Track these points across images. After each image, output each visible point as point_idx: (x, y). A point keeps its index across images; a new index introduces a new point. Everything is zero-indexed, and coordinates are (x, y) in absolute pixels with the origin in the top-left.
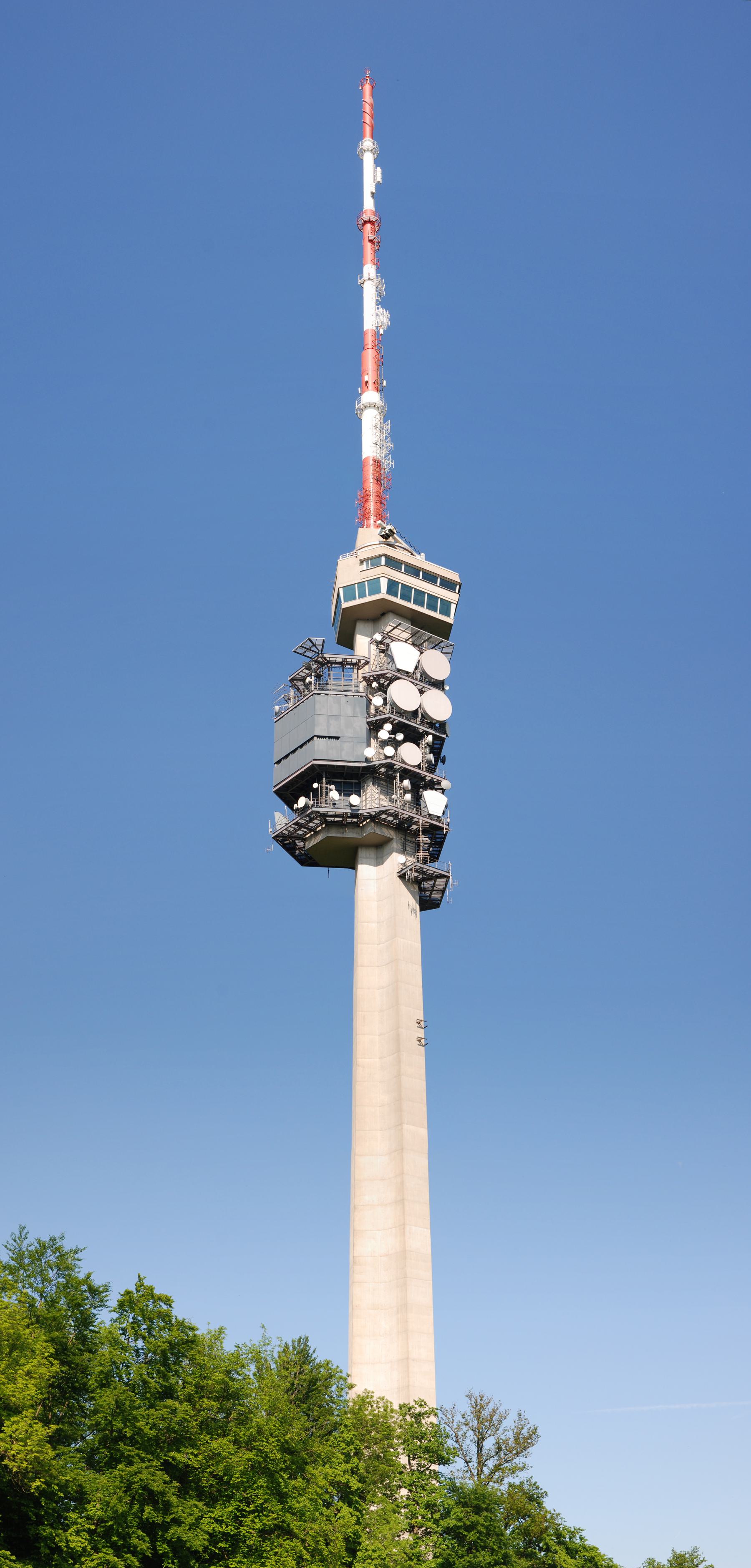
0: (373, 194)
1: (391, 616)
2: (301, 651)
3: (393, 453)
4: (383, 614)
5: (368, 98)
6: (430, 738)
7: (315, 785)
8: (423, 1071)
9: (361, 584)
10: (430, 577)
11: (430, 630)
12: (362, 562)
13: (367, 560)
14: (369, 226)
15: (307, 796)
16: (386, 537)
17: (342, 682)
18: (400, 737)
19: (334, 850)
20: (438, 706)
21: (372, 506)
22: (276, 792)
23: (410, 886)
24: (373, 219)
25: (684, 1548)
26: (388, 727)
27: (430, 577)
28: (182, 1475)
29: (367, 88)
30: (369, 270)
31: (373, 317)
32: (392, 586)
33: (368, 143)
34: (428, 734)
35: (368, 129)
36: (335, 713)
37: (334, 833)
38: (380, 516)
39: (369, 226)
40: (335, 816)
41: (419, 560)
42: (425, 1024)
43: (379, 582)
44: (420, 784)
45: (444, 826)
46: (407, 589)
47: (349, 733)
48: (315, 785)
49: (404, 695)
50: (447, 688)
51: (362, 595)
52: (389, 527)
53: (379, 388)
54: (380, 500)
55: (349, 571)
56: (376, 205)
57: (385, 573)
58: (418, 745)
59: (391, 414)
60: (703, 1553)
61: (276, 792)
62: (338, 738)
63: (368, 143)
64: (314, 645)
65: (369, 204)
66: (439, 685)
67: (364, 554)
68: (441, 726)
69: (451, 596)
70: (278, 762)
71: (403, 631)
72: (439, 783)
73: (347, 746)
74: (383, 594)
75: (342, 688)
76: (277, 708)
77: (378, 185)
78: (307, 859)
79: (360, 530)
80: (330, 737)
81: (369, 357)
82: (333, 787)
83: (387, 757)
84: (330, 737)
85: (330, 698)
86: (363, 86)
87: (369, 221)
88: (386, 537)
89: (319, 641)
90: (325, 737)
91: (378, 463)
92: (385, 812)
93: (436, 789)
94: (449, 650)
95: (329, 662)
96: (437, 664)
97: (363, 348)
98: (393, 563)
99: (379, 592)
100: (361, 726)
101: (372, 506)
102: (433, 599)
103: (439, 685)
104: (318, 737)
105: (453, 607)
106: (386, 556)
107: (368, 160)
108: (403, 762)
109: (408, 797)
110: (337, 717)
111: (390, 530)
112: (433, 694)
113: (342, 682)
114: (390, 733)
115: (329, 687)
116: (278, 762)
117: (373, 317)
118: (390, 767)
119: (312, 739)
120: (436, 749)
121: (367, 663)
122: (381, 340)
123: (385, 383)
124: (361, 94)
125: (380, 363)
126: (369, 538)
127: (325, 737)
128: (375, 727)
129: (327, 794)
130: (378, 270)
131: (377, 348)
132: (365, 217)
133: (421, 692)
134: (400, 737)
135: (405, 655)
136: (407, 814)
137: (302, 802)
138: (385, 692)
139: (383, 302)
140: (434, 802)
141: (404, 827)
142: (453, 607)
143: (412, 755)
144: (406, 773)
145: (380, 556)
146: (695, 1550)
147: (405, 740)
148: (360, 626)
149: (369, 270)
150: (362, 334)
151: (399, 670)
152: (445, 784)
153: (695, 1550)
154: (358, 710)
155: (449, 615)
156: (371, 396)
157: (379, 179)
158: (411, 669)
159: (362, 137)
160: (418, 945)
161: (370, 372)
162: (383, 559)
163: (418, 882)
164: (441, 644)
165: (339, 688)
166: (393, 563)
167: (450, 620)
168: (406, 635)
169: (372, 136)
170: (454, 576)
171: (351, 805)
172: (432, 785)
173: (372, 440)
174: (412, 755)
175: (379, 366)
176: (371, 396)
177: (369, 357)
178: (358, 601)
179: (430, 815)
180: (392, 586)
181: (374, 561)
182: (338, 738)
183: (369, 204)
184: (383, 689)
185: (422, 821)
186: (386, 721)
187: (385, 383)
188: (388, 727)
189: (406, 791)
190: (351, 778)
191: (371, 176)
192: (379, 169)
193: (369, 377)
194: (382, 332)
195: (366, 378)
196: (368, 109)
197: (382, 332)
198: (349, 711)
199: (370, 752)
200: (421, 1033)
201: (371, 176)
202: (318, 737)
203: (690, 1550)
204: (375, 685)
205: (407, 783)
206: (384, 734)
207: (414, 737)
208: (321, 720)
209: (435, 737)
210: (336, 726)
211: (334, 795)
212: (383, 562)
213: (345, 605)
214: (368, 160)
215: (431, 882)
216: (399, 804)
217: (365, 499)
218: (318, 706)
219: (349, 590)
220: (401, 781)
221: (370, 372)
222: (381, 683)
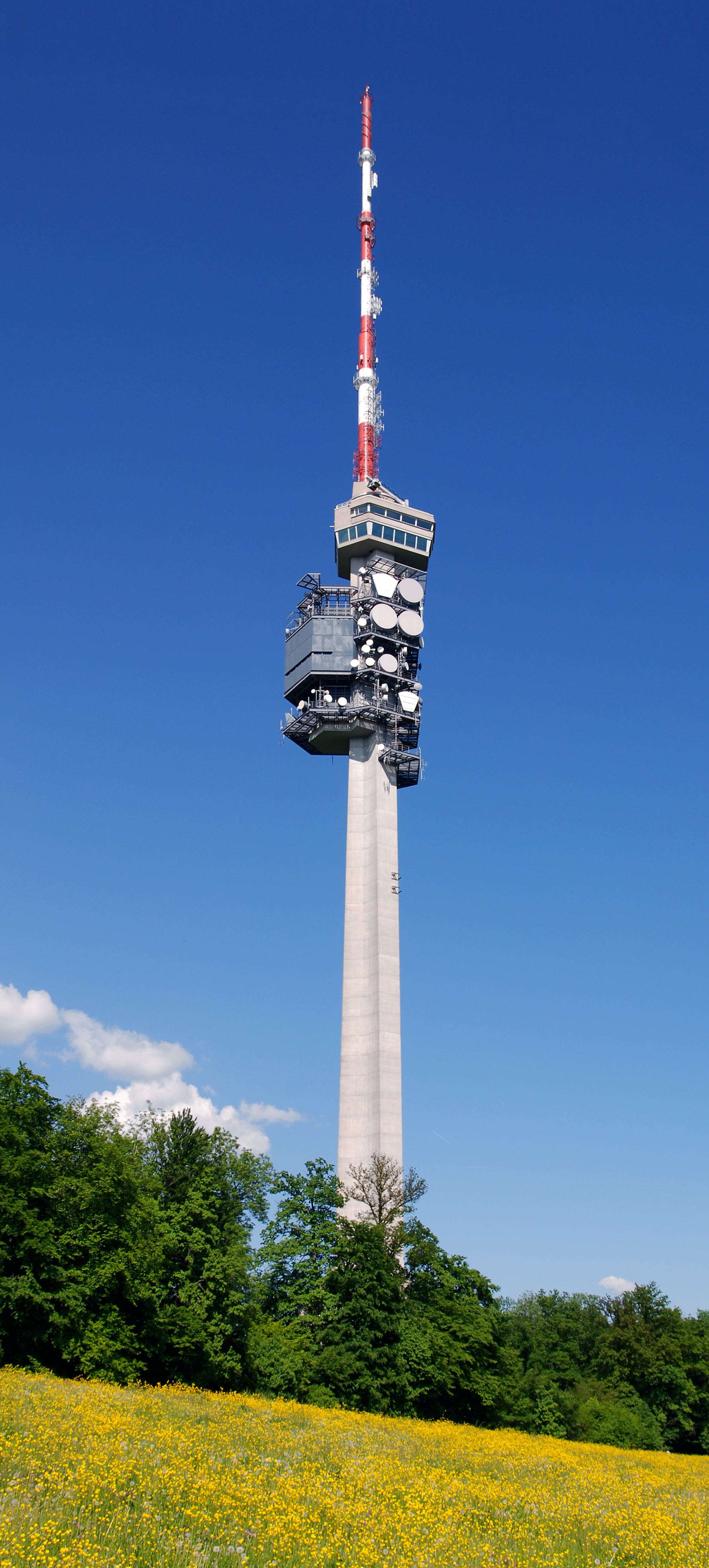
0: (369, 198)
1: (377, 551)
2: (304, 584)
3: (384, 419)
4: (371, 552)
5: (367, 112)
6: (405, 650)
7: (313, 691)
8: (397, 913)
9: (352, 529)
10: (409, 520)
11: (408, 562)
12: (352, 510)
13: (356, 508)
14: (366, 226)
15: (306, 700)
16: (373, 488)
17: (337, 608)
18: (381, 650)
19: (331, 742)
20: (413, 624)
21: (366, 464)
22: (287, 697)
23: (388, 767)
24: (369, 219)
25: (644, 1282)
26: (370, 642)
27: (409, 520)
28: (43, 1207)
29: (367, 101)
30: (366, 264)
31: (369, 304)
32: (377, 528)
33: (366, 152)
34: (403, 646)
35: (367, 140)
36: (329, 633)
37: (327, 728)
38: (372, 474)
39: (366, 226)
40: (328, 715)
41: (404, 507)
42: (402, 876)
43: (366, 526)
44: (395, 686)
45: (416, 720)
46: (389, 530)
47: (339, 649)
48: (313, 691)
49: (384, 616)
50: (421, 609)
51: (353, 537)
52: (374, 480)
53: (372, 365)
54: (372, 459)
55: (343, 517)
56: (372, 208)
57: (371, 519)
58: (396, 656)
59: (382, 386)
60: (659, 1286)
61: (287, 697)
62: (330, 653)
63: (366, 152)
64: (312, 579)
65: (366, 206)
66: (414, 607)
67: (355, 503)
68: (414, 640)
69: (428, 535)
70: (287, 674)
71: (383, 564)
72: (412, 685)
73: (338, 659)
74: (370, 535)
75: (337, 613)
76: (287, 630)
77: (374, 190)
78: (313, 749)
79: (355, 483)
80: (325, 653)
81: (366, 337)
82: (327, 692)
83: (369, 667)
84: (325, 653)
85: (325, 622)
86: (362, 100)
87: (368, 223)
88: (373, 488)
89: (316, 575)
90: (320, 653)
91: (371, 428)
92: (367, 710)
93: (412, 691)
94: (423, 578)
95: (326, 592)
96: (413, 590)
97: (360, 331)
98: (378, 510)
99: (366, 533)
100: (349, 641)
101: (366, 464)
102: (411, 537)
103: (414, 607)
104: (315, 653)
105: (429, 543)
106: (371, 504)
107: (366, 167)
108: (382, 670)
109: (386, 697)
110: (330, 636)
111: (376, 483)
112: (409, 614)
113: (337, 608)
114: (371, 647)
115: (325, 613)
116: (287, 674)
117: (369, 304)
118: (371, 674)
119: (310, 655)
120: (412, 658)
121: (357, 591)
122: (376, 324)
123: (377, 360)
124: (361, 108)
125: (373, 345)
126: (361, 490)
127: (320, 653)
128: (360, 643)
129: (322, 697)
130: (373, 265)
131: (371, 330)
132: (363, 219)
133: (398, 613)
134: (381, 650)
135: (385, 584)
136: (384, 711)
137: (302, 704)
138: (368, 614)
139: (376, 291)
140: (409, 701)
141: (382, 721)
142: (429, 543)
143: (389, 664)
144: (384, 679)
145: (366, 504)
146: (653, 1284)
147: (385, 652)
148: (354, 563)
149: (366, 264)
150: (360, 319)
151: (380, 597)
152: (418, 686)
153: (653, 1284)
154: (347, 630)
155: (425, 550)
156: (366, 372)
157: (375, 184)
158: (390, 595)
159: (361, 147)
160: (395, 814)
161: (366, 351)
162: (369, 507)
163: (394, 764)
164: (417, 574)
165: (334, 613)
166: (378, 510)
167: (426, 554)
168: (386, 568)
169: (370, 147)
170: (429, 517)
171: (340, 706)
172: (406, 687)
173: (366, 410)
174: (389, 664)
175: (372, 346)
176: (366, 372)
177: (366, 337)
178: (350, 542)
179: (404, 711)
180: (377, 528)
181: (362, 509)
182: (330, 653)
183: (366, 206)
184: (367, 612)
185: (396, 717)
186: (368, 637)
187: (377, 360)
188: (370, 642)
189: (384, 693)
190: (342, 685)
191: (369, 181)
192: (375, 175)
193: (365, 356)
194: (375, 317)
195: (361, 357)
196: (366, 122)
197: (375, 317)
198: (338, 631)
199: (355, 663)
200: (396, 884)
201: (369, 181)
202: (315, 653)
203: (649, 1284)
204: (360, 609)
205: (385, 686)
206: (366, 649)
207: (392, 650)
208: (318, 639)
209: (409, 649)
210: (331, 644)
211: (328, 698)
212: (369, 510)
213: (340, 546)
214: (366, 167)
215: (407, 764)
216: (378, 704)
217: (360, 458)
218: (314, 629)
219: (343, 533)
220: (380, 685)
221: (366, 351)
222: (365, 607)
